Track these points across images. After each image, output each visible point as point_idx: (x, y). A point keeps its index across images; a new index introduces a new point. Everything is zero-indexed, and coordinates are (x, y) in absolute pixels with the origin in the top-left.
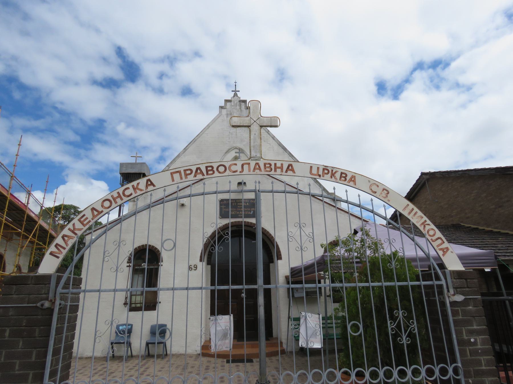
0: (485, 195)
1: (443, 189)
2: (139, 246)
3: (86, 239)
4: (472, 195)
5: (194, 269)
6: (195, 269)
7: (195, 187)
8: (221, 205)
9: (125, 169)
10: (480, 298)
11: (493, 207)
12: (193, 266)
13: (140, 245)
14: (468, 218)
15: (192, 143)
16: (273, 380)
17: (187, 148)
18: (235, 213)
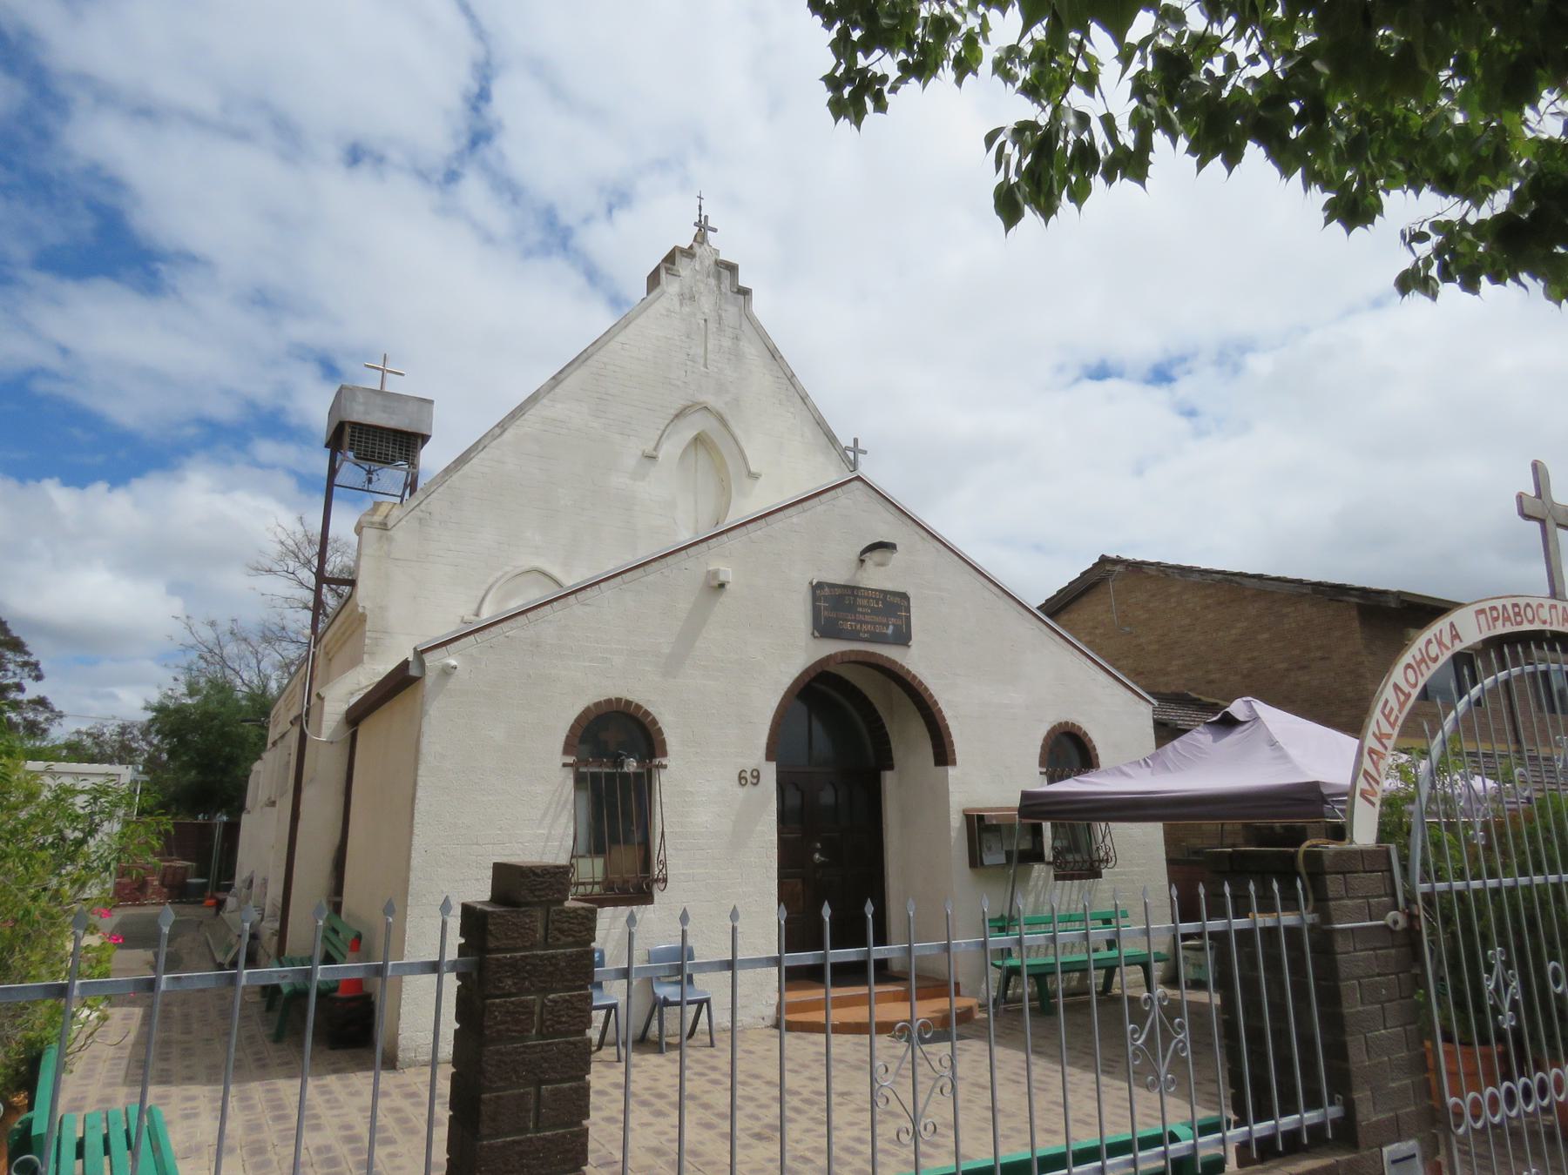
0: (1266, 636)
1: (1151, 605)
2: (596, 701)
3: (427, 664)
4: (1233, 632)
5: (752, 783)
6: (755, 781)
7: (748, 533)
8: (815, 599)
9: (361, 408)
10: (1302, 881)
11: (1284, 666)
12: (749, 773)
13: (602, 699)
14: (1210, 682)
15: (576, 364)
16: (286, 1112)
17: (562, 376)
18: (851, 625)
